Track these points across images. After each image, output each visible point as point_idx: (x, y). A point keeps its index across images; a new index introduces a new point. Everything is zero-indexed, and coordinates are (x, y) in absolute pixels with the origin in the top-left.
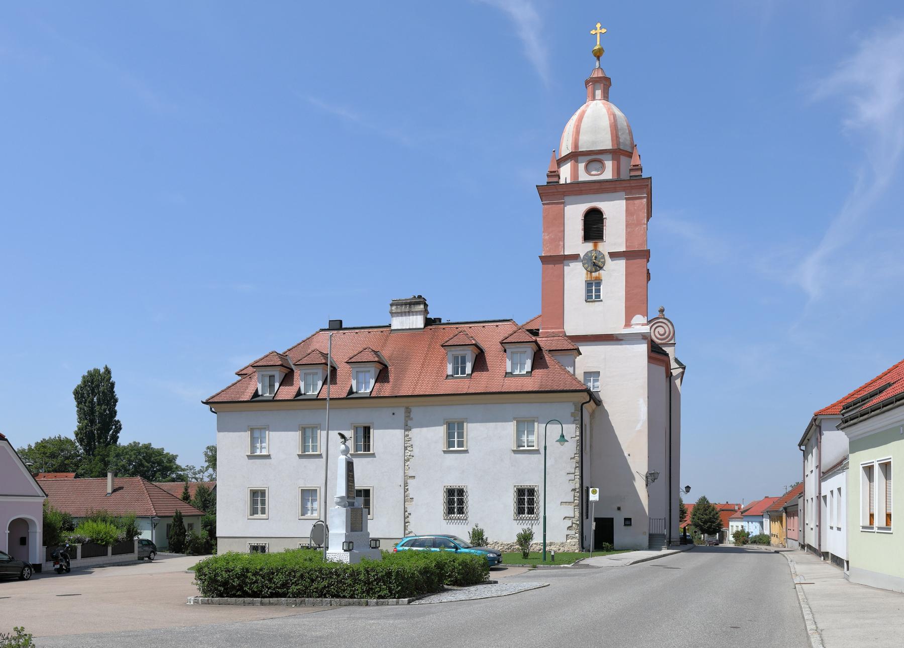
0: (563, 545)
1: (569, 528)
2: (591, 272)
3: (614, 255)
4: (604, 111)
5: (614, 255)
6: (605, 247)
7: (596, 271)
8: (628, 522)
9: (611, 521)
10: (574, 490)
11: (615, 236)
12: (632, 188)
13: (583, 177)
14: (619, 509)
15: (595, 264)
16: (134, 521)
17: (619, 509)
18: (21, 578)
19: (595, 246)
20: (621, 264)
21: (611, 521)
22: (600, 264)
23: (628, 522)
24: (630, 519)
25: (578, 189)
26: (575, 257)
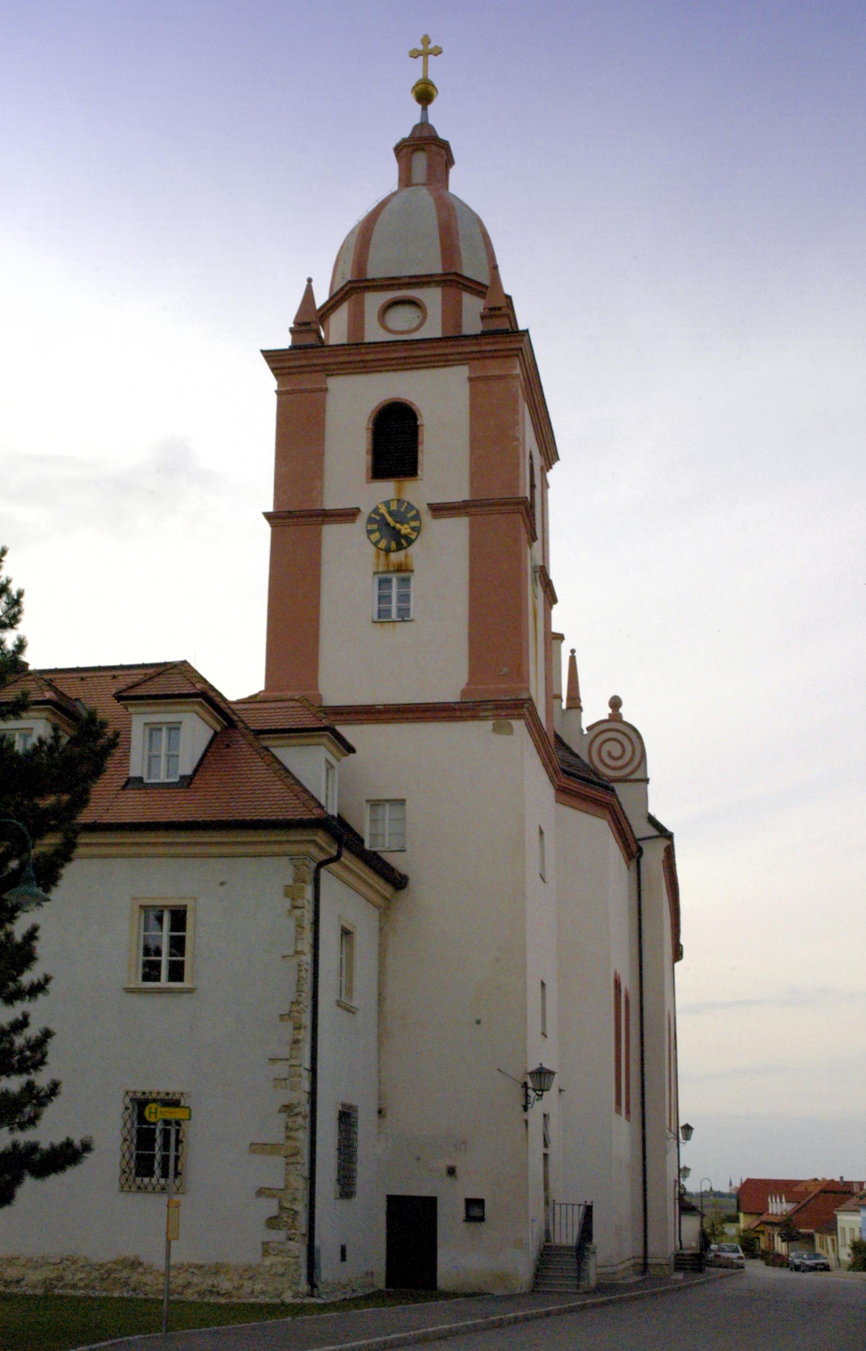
0: (250, 1273)
1: (272, 1223)
2: (388, 551)
3: (439, 510)
4: (431, 200)
5: (439, 510)
6: (420, 492)
7: (400, 547)
8: (475, 1210)
9: (429, 1205)
10: (287, 1108)
11: (445, 463)
12: (483, 356)
13: (374, 333)
14: (451, 1171)
15: (394, 534)
16: (681, 1187)
17: (451, 1171)
18: (591, 1216)
19: (399, 491)
20: (458, 528)
21: (429, 1205)
22: (405, 529)
23: (475, 1212)
24: (480, 1203)
25: (361, 357)
26: (349, 515)
